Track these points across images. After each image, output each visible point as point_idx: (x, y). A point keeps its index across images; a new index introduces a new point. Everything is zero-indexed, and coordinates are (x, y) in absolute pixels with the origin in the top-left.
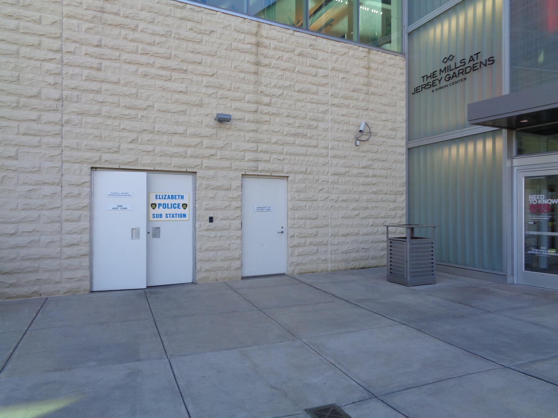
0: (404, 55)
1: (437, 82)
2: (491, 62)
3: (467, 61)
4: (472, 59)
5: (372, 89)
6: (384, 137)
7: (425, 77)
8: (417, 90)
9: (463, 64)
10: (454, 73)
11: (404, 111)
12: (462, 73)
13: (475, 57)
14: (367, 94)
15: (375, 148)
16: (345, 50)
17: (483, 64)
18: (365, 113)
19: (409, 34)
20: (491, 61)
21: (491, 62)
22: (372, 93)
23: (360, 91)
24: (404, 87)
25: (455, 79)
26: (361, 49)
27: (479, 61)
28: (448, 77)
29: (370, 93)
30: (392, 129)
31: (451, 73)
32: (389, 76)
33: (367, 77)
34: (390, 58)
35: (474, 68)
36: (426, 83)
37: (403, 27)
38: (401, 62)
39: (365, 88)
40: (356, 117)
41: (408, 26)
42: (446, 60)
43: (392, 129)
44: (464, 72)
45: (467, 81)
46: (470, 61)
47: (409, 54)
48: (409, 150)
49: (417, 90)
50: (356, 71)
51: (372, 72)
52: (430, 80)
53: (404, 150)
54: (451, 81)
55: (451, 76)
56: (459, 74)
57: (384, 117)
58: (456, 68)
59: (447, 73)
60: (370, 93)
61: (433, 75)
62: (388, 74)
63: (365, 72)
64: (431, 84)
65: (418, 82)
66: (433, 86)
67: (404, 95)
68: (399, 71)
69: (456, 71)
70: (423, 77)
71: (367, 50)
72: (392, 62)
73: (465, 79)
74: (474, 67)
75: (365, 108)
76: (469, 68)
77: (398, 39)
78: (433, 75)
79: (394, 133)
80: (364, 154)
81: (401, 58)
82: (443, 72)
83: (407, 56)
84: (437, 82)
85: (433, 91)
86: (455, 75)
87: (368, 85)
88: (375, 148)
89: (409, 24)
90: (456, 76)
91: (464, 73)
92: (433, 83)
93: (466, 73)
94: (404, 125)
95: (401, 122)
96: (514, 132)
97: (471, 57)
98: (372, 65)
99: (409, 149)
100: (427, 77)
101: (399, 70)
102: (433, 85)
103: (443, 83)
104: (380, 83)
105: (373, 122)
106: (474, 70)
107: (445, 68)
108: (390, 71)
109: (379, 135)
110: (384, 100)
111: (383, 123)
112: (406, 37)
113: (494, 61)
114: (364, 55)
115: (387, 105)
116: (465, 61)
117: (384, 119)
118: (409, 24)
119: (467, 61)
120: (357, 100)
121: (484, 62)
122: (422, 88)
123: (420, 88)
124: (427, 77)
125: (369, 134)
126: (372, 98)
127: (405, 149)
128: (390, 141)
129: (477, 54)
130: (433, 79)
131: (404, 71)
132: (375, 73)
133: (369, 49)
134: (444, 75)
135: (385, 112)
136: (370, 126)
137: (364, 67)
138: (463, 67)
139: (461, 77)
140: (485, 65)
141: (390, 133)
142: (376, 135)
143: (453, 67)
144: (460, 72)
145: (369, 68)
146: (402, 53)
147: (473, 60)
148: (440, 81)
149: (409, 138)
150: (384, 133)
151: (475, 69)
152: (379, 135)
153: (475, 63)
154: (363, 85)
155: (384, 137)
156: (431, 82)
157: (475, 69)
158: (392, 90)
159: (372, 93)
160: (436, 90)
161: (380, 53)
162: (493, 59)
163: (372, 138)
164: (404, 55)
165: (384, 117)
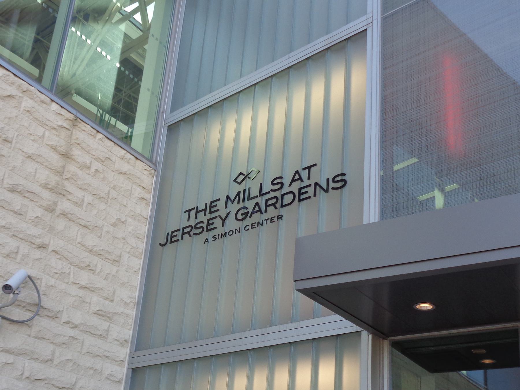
0: (155, 165)
1: (218, 222)
2: (339, 185)
3: (287, 181)
4: (297, 177)
5: (65, 205)
6: (76, 327)
7: (193, 213)
8: (171, 239)
9: (279, 186)
10: (257, 204)
11: (137, 281)
12: (274, 205)
13: (304, 174)
14: (50, 210)
15: (45, 349)
16: (11, 90)
17: (321, 187)
18: (37, 254)
19: (173, 128)
20: (340, 181)
21: (339, 185)
22: (64, 215)
23: (31, 197)
24: (144, 229)
25: (256, 218)
26: (54, 107)
27: (312, 182)
28: (241, 212)
29: (58, 212)
30: (100, 314)
31: (250, 205)
32: (113, 194)
33: (60, 173)
34: (122, 158)
35: (301, 196)
36: (192, 222)
37: (159, 113)
38: (145, 177)
39: (46, 194)
40: (8, 256)
41: (171, 112)
42: (242, 177)
43: (100, 314)
44: (279, 203)
45: (282, 222)
46: (293, 180)
47: (165, 167)
48: (135, 372)
49: (171, 239)
50: (31, 148)
51: (72, 168)
52: (202, 217)
53: (122, 372)
54: (248, 221)
55: (250, 210)
56: (267, 206)
57: (84, 278)
58: (261, 195)
59: (242, 205)
60: (58, 212)
61: (211, 207)
62: (114, 188)
63: (55, 160)
64: (205, 225)
65: (176, 221)
66: (208, 230)
67: (142, 246)
68: (138, 192)
69: (262, 201)
70: (189, 211)
71: (71, 116)
72: (125, 167)
73: (280, 217)
74: (300, 194)
75: (39, 241)
76: (291, 196)
77: (146, 134)
78: (212, 207)
79: (105, 325)
80: (10, 359)
81: (147, 168)
82: (233, 202)
83: (160, 169)
84: (218, 222)
85: (207, 241)
86: (258, 209)
87: (58, 191)
88: (45, 349)
89: (174, 108)
90: (260, 210)
91: (278, 205)
92: (208, 225)
93: (282, 206)
94: (132, 312)
95: (126, 304)
96: (386, 345)
97: (297, 172)
98: (76, 152)
99: (134, 370)
100: (197, 212)
101: (139, 190)
102: (209, 227)
103: (232, 224)
104: (88, 198)
105: (52, 282)
106: (300, 200)
107: (239, 194)
108: (118, 193)
109: (64, 318)
110: (91, 241)
111: (81, 293)
112: (164, 131)
113: (345, 181)
114: (60, 123)
115: (99, 255)
116: (283, 181)
117: (83, 283)
118: (174, 108)
119: (287, 181)
120: (18, 214)
121: (324, 185)
122: (183, 234)
123: (180, 234)
124: (197, 212)
125: (35, 309)
126: (61, 224)
127: (125, 370)
128: (89, 340)
129: (309, 168)
130: (208, 216)
131: (150, 197)
132: (80, 172)
133: (76, 117)
134: (234, 208)
135: (88, 268)
136: (42, 289)
137: (54, 149)
138: (278, 194)
139: (272, 212)
140: (326, 191)
141: (95, 321)
142: (55, 316)
143: (255, 192)
144: (270, 202)
145: (66, 156)
146: (151, 160)
147: (301, 179)
148: (224, 220)
149: (140, 343)
150: (77, 318)
151: (302, 197)
152: (64, 318)
153: (303, 185)
154: (45, 186)
155: (76, 327)
156: (205, 222)
157: (302, 197)
158: (114, 225)
159: (64, 215)
160: (215, 238)
161: (100, 136)
162: (344, 178)
163: (42, 323)
164: (155, 165)
165: (84, 278)
